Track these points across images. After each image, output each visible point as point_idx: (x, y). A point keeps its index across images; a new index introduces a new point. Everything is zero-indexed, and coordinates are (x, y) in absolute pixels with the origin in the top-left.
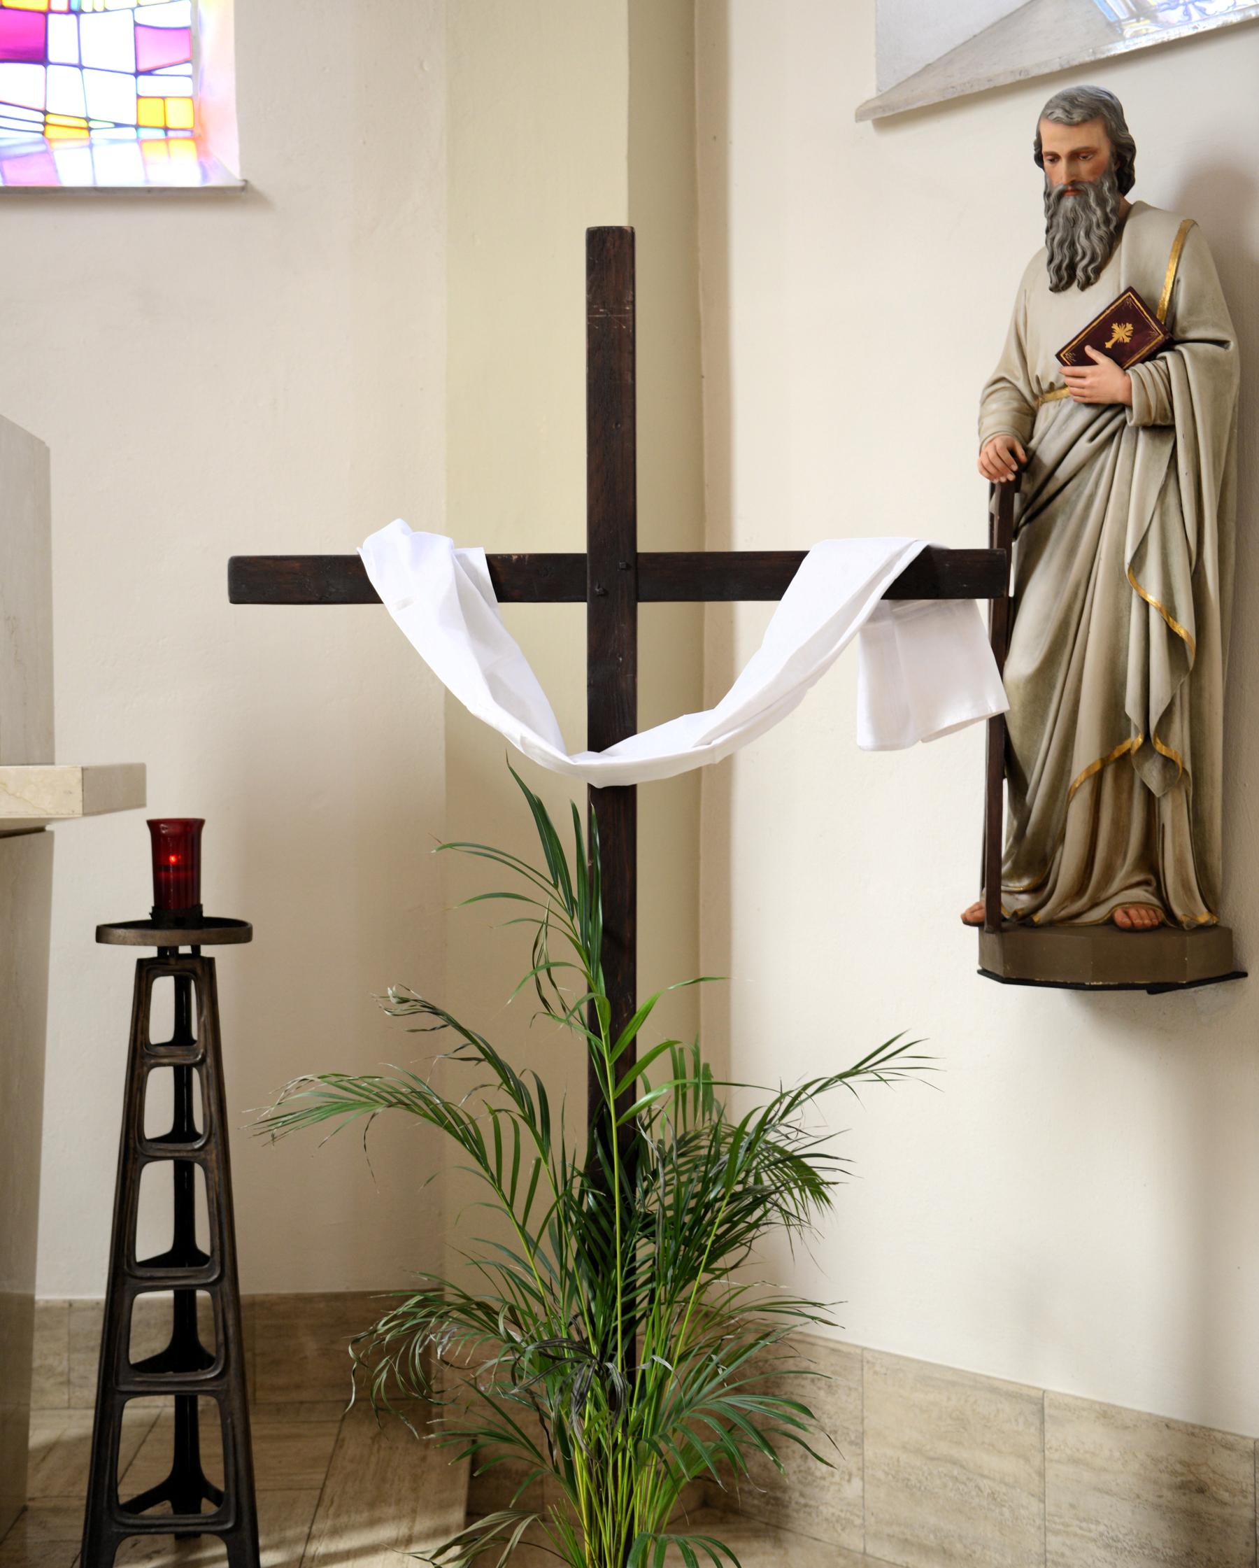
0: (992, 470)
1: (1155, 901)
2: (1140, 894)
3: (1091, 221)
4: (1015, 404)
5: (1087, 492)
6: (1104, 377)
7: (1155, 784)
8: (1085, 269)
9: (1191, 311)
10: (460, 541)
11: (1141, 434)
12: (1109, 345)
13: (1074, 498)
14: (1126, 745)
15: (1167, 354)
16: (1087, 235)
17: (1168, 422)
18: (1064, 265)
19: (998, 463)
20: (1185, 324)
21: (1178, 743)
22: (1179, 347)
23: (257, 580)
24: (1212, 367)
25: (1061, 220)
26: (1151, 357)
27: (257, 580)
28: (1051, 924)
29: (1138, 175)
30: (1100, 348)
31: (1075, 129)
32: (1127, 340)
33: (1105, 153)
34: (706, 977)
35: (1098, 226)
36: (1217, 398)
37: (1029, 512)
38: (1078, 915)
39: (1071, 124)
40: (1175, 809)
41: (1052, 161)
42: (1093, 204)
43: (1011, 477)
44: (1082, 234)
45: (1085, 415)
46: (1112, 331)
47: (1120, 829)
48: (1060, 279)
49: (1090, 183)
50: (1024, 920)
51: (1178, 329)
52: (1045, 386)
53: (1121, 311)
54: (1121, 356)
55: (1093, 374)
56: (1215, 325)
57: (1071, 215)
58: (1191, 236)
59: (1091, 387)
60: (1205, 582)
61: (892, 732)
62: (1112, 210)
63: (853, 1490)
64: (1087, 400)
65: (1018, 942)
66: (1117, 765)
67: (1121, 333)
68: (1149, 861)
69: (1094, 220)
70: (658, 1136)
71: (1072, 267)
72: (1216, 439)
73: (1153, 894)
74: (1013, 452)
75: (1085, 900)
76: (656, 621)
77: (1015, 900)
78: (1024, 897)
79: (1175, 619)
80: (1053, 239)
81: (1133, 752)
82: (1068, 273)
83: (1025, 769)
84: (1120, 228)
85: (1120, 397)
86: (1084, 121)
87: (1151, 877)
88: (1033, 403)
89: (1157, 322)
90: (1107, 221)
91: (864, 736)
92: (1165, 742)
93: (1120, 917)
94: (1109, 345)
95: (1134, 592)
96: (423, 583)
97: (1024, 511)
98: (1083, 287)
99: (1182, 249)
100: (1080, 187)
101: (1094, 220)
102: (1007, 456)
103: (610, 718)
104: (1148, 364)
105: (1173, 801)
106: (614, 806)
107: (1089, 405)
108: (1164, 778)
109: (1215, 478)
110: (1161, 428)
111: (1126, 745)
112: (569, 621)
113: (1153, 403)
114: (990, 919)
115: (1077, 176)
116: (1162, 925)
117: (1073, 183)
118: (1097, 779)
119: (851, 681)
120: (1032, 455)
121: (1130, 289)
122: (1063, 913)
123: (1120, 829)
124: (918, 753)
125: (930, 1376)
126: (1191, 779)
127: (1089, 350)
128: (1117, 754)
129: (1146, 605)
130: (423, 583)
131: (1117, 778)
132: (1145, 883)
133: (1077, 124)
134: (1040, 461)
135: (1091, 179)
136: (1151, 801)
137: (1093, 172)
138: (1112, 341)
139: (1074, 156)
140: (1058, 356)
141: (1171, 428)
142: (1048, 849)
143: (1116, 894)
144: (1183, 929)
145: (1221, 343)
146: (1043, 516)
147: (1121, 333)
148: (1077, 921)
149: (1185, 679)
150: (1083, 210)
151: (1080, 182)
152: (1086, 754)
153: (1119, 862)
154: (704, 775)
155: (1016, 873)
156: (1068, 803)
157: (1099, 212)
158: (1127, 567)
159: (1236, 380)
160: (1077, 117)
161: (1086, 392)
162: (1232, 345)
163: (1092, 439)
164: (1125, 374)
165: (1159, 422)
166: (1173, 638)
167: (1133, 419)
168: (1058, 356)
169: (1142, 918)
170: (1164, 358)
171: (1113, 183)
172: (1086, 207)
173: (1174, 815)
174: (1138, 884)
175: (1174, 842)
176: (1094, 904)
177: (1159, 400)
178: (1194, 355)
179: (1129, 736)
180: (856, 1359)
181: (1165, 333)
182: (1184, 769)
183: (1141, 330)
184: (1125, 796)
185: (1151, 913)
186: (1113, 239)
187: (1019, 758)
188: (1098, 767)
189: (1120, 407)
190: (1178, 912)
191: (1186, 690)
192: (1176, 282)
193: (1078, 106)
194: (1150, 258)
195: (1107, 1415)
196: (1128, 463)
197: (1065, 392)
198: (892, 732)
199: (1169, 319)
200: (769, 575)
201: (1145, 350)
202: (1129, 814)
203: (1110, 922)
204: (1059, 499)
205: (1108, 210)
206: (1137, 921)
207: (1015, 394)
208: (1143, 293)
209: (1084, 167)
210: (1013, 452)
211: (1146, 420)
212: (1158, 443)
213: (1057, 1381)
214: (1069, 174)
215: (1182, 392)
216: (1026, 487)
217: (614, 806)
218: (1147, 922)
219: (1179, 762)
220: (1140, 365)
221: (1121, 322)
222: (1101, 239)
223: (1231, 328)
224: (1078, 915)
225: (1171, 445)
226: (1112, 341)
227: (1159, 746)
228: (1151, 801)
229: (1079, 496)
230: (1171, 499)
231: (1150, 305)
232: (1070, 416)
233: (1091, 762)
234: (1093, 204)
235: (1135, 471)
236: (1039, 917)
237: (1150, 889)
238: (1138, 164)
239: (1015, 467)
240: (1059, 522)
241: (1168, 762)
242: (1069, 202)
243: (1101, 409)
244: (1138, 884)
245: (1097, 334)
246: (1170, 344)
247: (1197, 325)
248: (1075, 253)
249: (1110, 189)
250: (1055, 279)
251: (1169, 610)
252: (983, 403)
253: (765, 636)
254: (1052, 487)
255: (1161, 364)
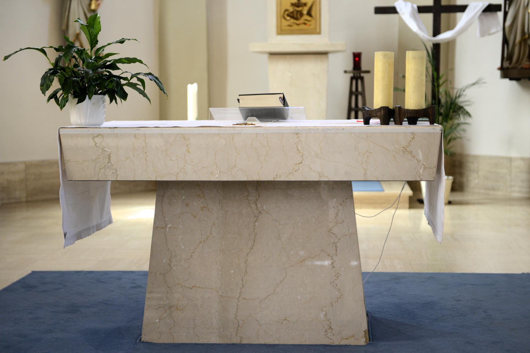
10: (412, 3)
23: (379, 10)
27: (379, 10)
28: (512, 68)
34: (451, 69)
50: (507, 68)
61: (484, 33)
63: (476, 181)
65: (506, 72)
66: (524, 40)
70: (443, 100)
76: (444, 16)
77: (506, 64)
91: (478, 34)
96: (406, 11)
103: (436, 32)
106: (437, 47)
112: (430, 17)
114: (502, 68)
118: (520, 43)
119: (476, 27)
124: (487, 38)
125: (491, 158)
130: (406, 11)
154: (50, 83)
155: (507, 60)
180: (476, 157)
195: (522, 159)
198: (484, 33)
200: (463, 8)
213: (514, 154)
217: (437, 47)
253: (462, 19)
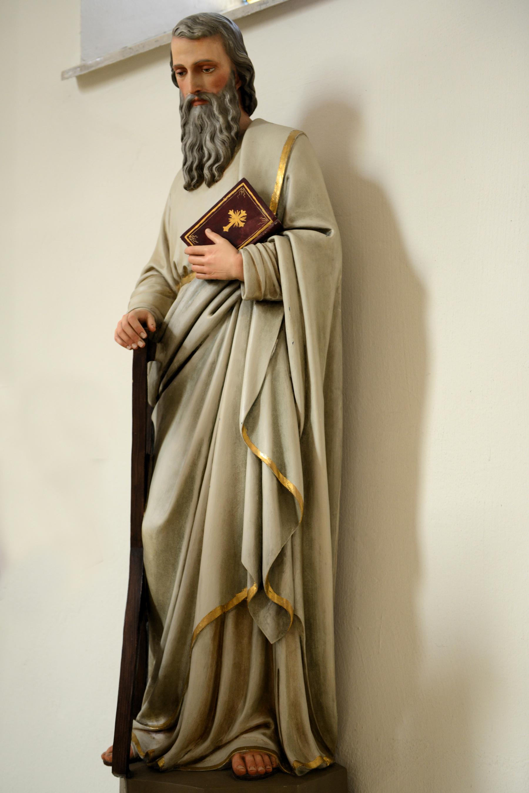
0: (125, 338)
1: (272, 745)
2: (258, 738)
3: (215, 127)
4: (158, 288)
5: (210, 360)
6: (221, 256)
7: (269, 632)
8: (211, 168)
9: (298, 203)
11: (255, 308)
12: (226, 229)
13: (200, 366)
14: (242, 596)
15: (276, 237)
16: (212, 139)
17: (278, 298)
18: (195, 165)
19: (129, 331)
20: (293, 215)
21: (289, 591)
22: (287, 233)
24: (314, 250)
25: (191, 128)
26: (263, 239)
28: (175, 769)
29: (259, 95)
30: (219, 231)
31: (196, 43)
32: (242, 225)
33: (225, 68)
35: (221, 131)
36: (320, 279)
37: (165, 380)
38: (202, 758)
39: (193, 38)
40: (289, 654)
41: (181, 74)
42: (216, 113)
43: (141, 344)
44: (208, 138)
45: (208, 290)
46: (229, 216)
47: (241, 671)
48: (192, 179)
49: (214, 95)
51: (287, 218)
52: (180, 270)
53: (236, 200)
54: (236, 239)
55: (210, 252)
56: (319, 216)
57: (198, 123)
58: (300, 142)
59: (209, 264)
60: (313, 443)
62: (232, 119)
64: (207, 276)
66: (236, 612)
67: (237, 218)
68: (267, 702)
69: (218, 126)
71: (201, 167)
72: (320, 316)
73: (270, 738)
74: (144, 323)
75: (207, 743)
78: (160, 737)
79: (285, 475)
80: (185, 145)
81: (249, 600)
82: (197, 176)
83: (161, 613)
84: (240, 136)
85: (234, 274)
86: (203, 37)
87: (270, 720)
88: (175, 288)
89: (270, 212)
90: (229, 128)
92: (277, 591)
93: (237, 766)
94: (226, 229)
95: (249, 449)
97: (161, 378)
98: (209, 185)
99: (291, 151)
100: (205, 97)
101: (218, 126)
102: (137, 325)
104: (259, 245)
105: (288, 646)
107: (211, 281)
108: (278, 624)
109: (320, 350)
110: (271, 303)
111: (242, 596)
113: (262, 278)
115: (202, 86)
116: (277, 770)
117: (198, 93)
118: (219, 624)
120: (162, 327)
121: (244, 180)
122: (187, 757)
123: (241, 671)
126: (305, 627)
127: (208, 233)
128: (235, 602)
129: (260, 462)
131: (237, 624)
132: (265, 725)
133: (198, 39)
134: (171, 333)
135: (215, 91)
136: (268, 649)
137: (216, 84)
138: (230, 225)
139: (199, 68)
140: (183, 237)
141: (280, 303)
142: (179, 691)
143: (237, 737)
144: (295, 776)
145: (324, 231)
146: (175, 382)
147: (237, 218)
148: (200, 765)
149: (297, 530)
150: (209, 117)
151: (205, 93)
152: (207, 603)
153: (240, 705)
156: (192, 648)
157: (221, 120)
158: (241, 426)
159: (338, 264)
160: (198, 32)
161: (205, 269)
162: (333, 232)
163: (213, 312)
164: (238, 252)
165: (269, 297)
166: (282, 492)
167: (245, 292)
168: (183, 237)
169: (257, 764)
170: (273, 241)
171: (234, 96)
172: (211, 115)
173: (288, 660)
174: (257, 727)
175: (288, 687)
176: (217, 748)
177: (268, 277)
178: (299, 239)
179: (245, 586)
181: (274, 219)
182: (296, 616)
183: (253, 215)
184: (245, 640)
185: (266, 758)
186: (235, 143)
187: (156, 604)
188: (218, 613)
189: (235, 283)
190: (291, 758)
191: (298, 541)
192: (285, 179)
193: (199, 24)
194: (264, 160)
196: (244, 334)
197: (195, 274)
199: (280, 211)
201: (257, 234)
202: (249, 659)
203: (228, 766)
204: (188, 366)
205: (230, 118)
206: (252, 769)
207: (160, 280)
208: (258, 188)
209: (208, 80)
210: (144, 323)
211: (257, 294)
212: (269, 315)
214: (194, 85)
215: (287, 270)
216: (159, 355)
218: (261, 769)
219: (291, 612)
220: (252, 246)
221: (248, 218)
222: (223, 142)
223: (332, 219)
224: (202, 758)
225: (280, 318)
226: (230, 225)
227: (271, 594)
228: (268, 649)
229: (204, 364)
230: (281, 366)
231: (264, 198)
232: (195, 293)
233: (211, 609)
234: (216, 113)
235: (250, 338)
236: (163, 762)
237: (268, 732)
238: (258, 84)
239: (144, 335)
240: (189, 387)
241: (280, 610)
242: (197, 111)
243: (221, 286)
244: (257, 727)
245: (216, 220)
246: (279, 229)
247: (302, 216)
248: (203, 156)
249: (231, 101)
250: (187, 178)
251: (280, 466)
252: (137, 286)
254: (181, 356)
255: (270, 245)
